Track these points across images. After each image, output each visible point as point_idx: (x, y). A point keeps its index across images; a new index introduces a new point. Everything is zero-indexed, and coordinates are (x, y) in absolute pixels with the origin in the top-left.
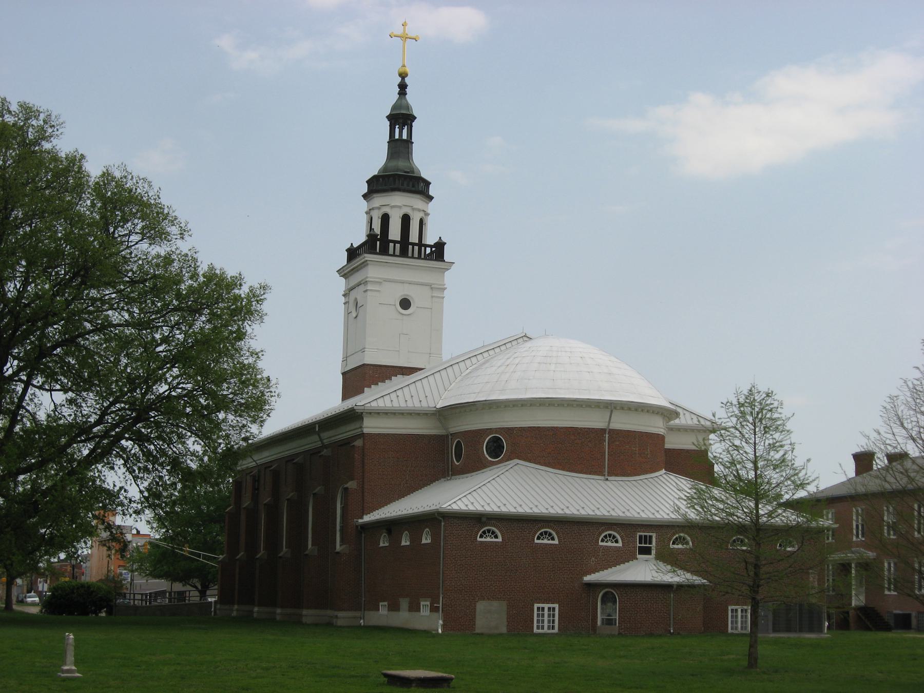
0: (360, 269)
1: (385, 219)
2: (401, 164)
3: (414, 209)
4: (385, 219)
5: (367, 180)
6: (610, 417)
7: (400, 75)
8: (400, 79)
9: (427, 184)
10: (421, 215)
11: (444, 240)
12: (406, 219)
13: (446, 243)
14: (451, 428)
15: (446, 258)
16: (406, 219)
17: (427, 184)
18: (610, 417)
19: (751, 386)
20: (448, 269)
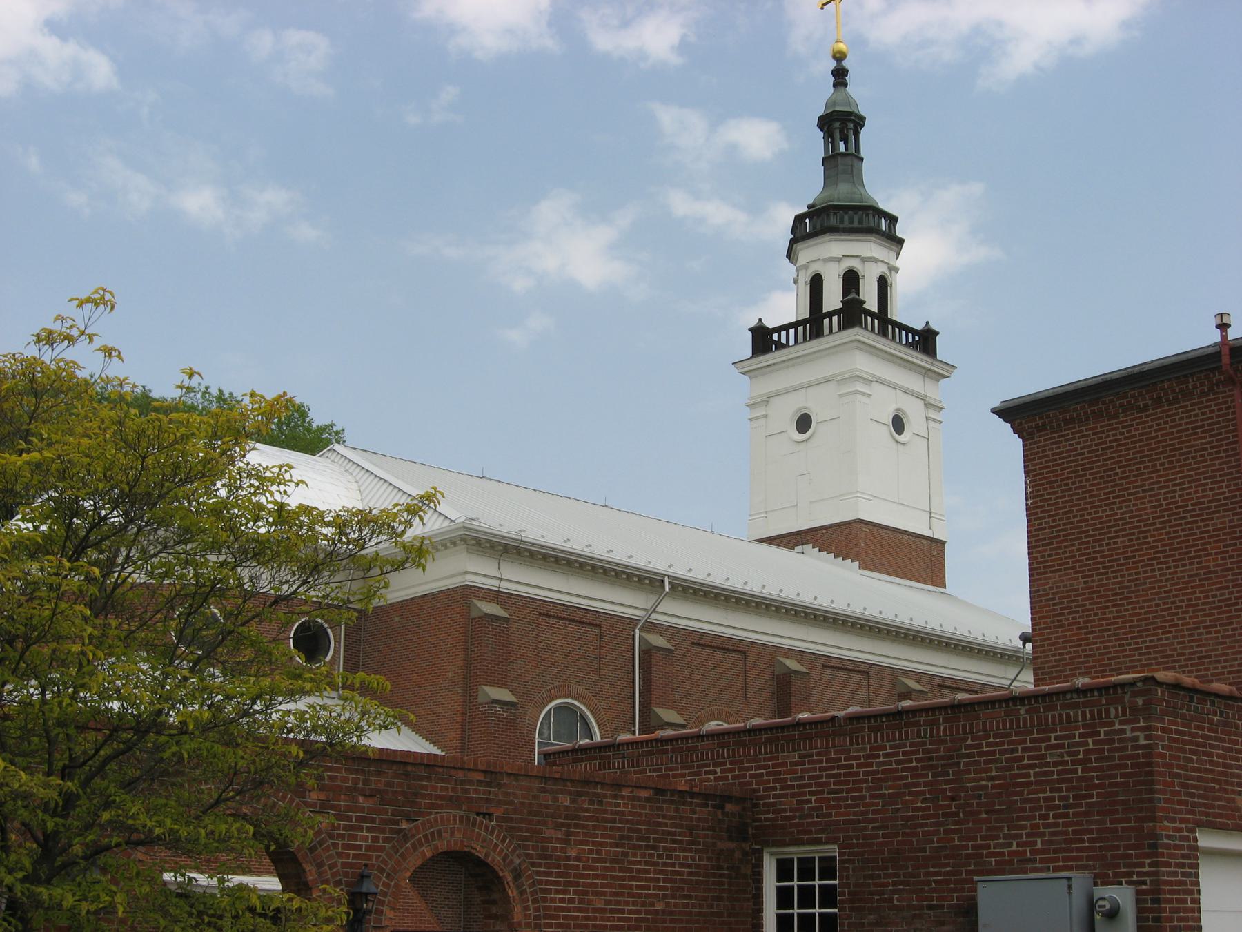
0: (788, 367)
1: (816, 283)
2: (843, 192)
3: (864, 260)
4: (816, 283)
5: (948, 550)
6: (1018, 674)
7: (834, 57)
8: (834, 64)
9: (893, 220)
10: (881, 269)
11: (934, 326)
12: (851, 280)
13: (938, 333)
14: (436, 520)
15: (940, 355)
16: (851, 280)
17: (893, 220)
18: (1018, 674)
19: (330, 423)
20: (945, 377)
